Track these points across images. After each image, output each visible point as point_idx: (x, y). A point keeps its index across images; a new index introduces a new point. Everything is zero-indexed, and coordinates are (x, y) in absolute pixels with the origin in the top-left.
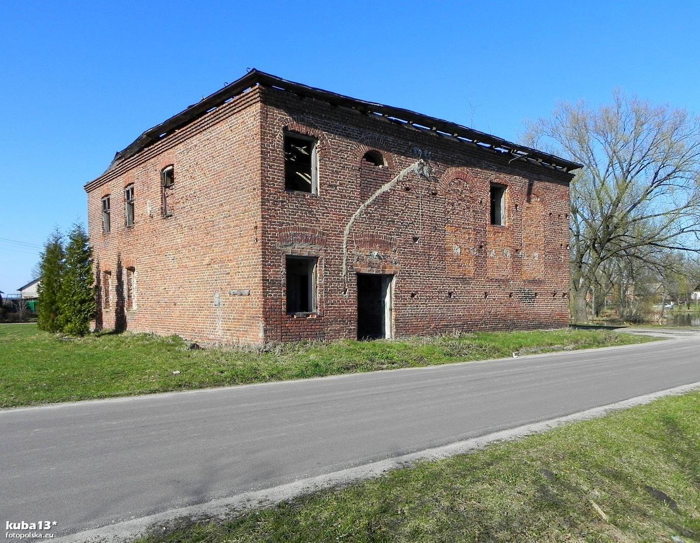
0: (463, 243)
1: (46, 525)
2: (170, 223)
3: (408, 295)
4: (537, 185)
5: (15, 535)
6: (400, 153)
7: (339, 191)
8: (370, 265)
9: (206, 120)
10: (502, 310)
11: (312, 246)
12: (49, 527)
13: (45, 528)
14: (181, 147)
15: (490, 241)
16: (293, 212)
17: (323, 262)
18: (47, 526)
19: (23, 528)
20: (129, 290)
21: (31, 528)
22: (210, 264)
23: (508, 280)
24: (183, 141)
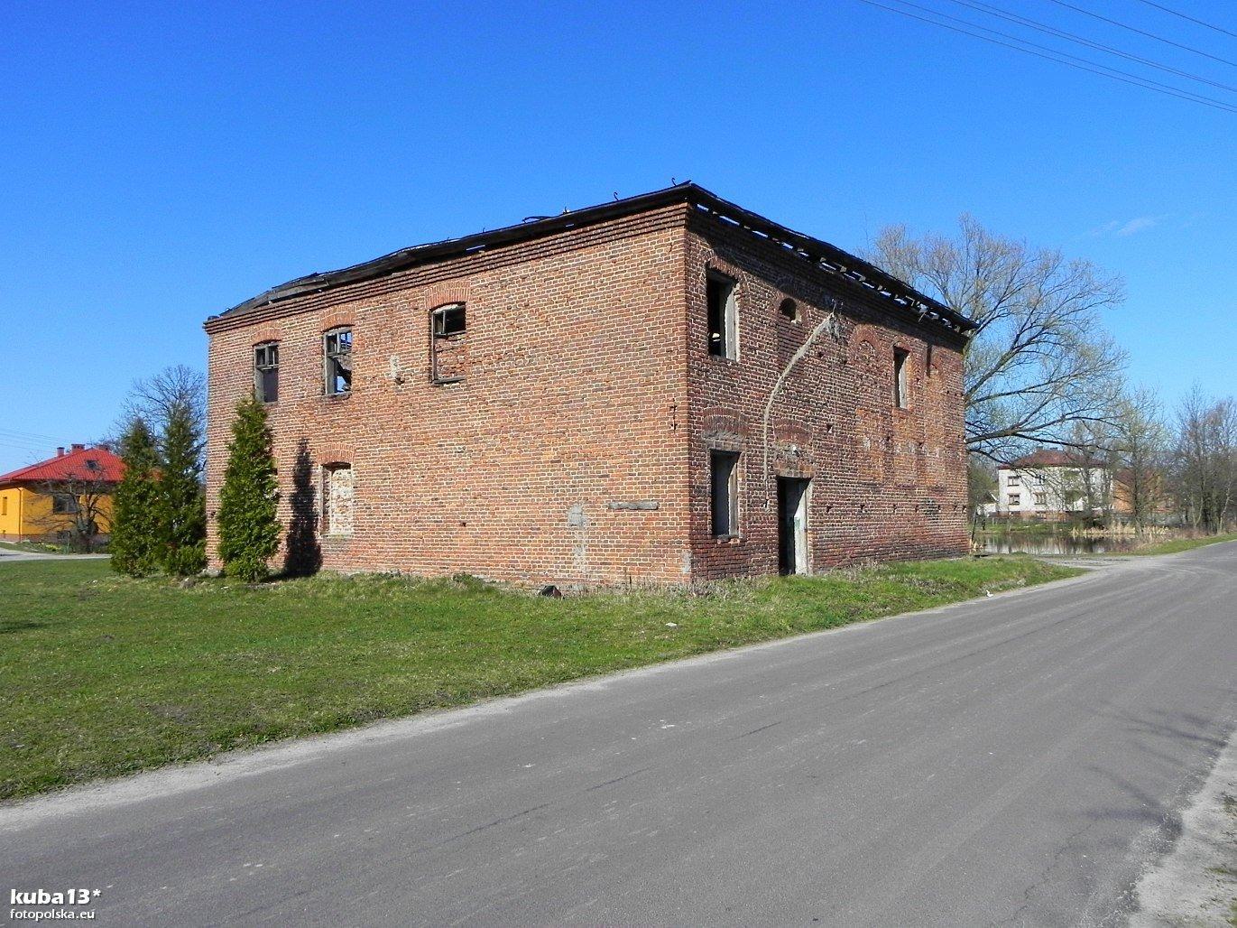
0: (873, 434)
1: (81, 896)
2: (454, 397)
3: (821, 509)
4: (936, 351)
5: (27, 914)
6: (814, 304)
7: (758, 357)
8: (789, 464)
10: (908, 530)
11: (735, 436)
12: (87, 900)
13: (80, 902)
14: (486, 278)
15: (896, 430)
16: (716, 386)
17: (746, 461)
18: (83, 898)
19: (40, 901)
20: (325, 501)
21: (54, 901)
22: (559, 461)
23: (913, 487)
24: (492, 269)
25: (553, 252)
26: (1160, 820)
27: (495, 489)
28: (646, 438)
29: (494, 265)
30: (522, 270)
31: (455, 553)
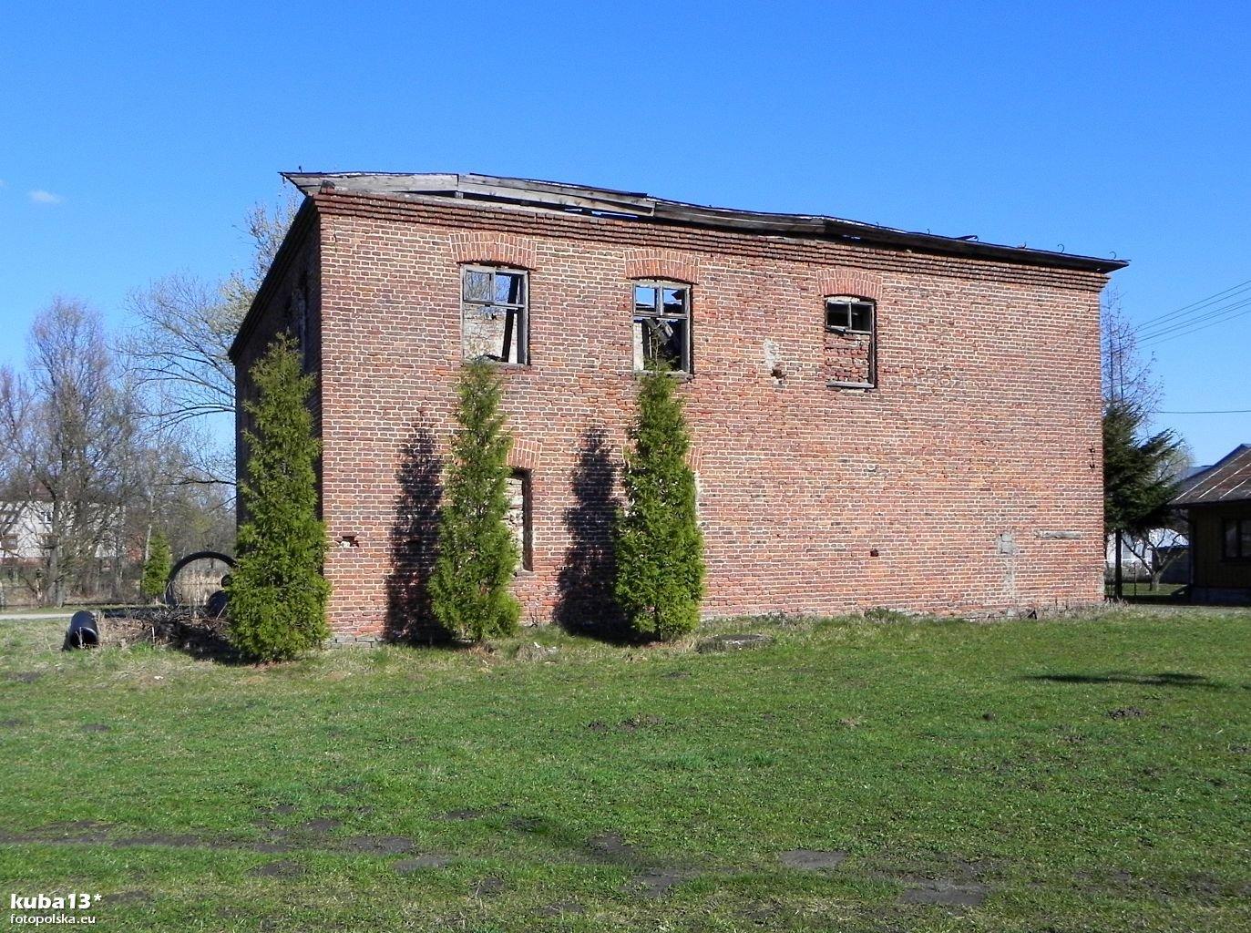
1: (82, 901)
12: (88, 905)
13: (81, 906)
14: (903, 280)
18: (84, 903)
21: (55, 906)
25: (984, 277)
27: (916, 514)
28: (1070, 474)
29: (915, 270)
30: (946, 284)
31: (865, 585)
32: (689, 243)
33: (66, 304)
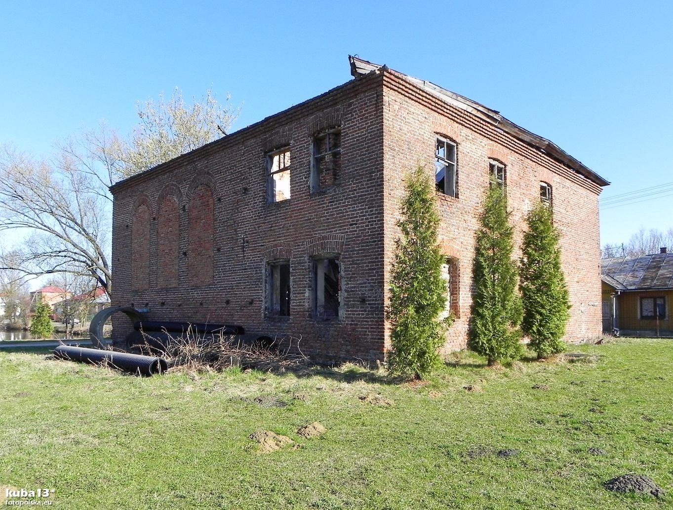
1: (45, 492)
9: (562, 172)
13: (44, 496)
18: (45, 494)
19: (22, 495)
26: (460, 365)
32: (506, 144)
33: (27, 239)
